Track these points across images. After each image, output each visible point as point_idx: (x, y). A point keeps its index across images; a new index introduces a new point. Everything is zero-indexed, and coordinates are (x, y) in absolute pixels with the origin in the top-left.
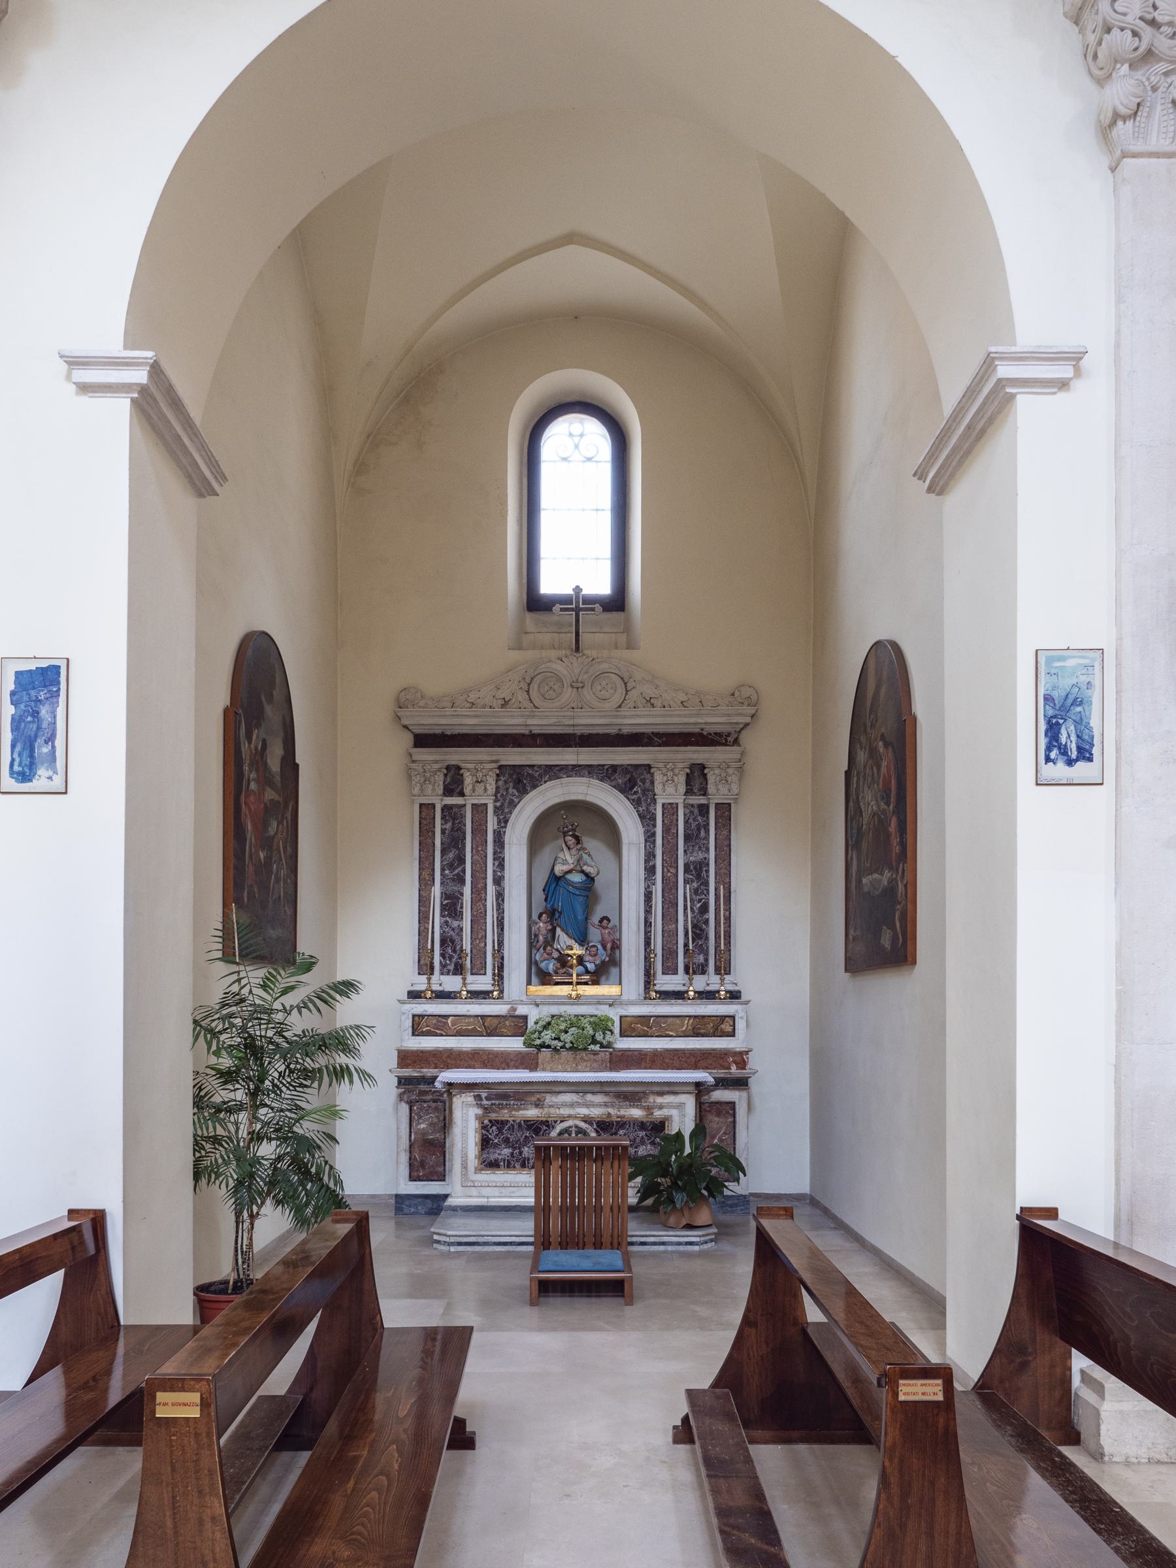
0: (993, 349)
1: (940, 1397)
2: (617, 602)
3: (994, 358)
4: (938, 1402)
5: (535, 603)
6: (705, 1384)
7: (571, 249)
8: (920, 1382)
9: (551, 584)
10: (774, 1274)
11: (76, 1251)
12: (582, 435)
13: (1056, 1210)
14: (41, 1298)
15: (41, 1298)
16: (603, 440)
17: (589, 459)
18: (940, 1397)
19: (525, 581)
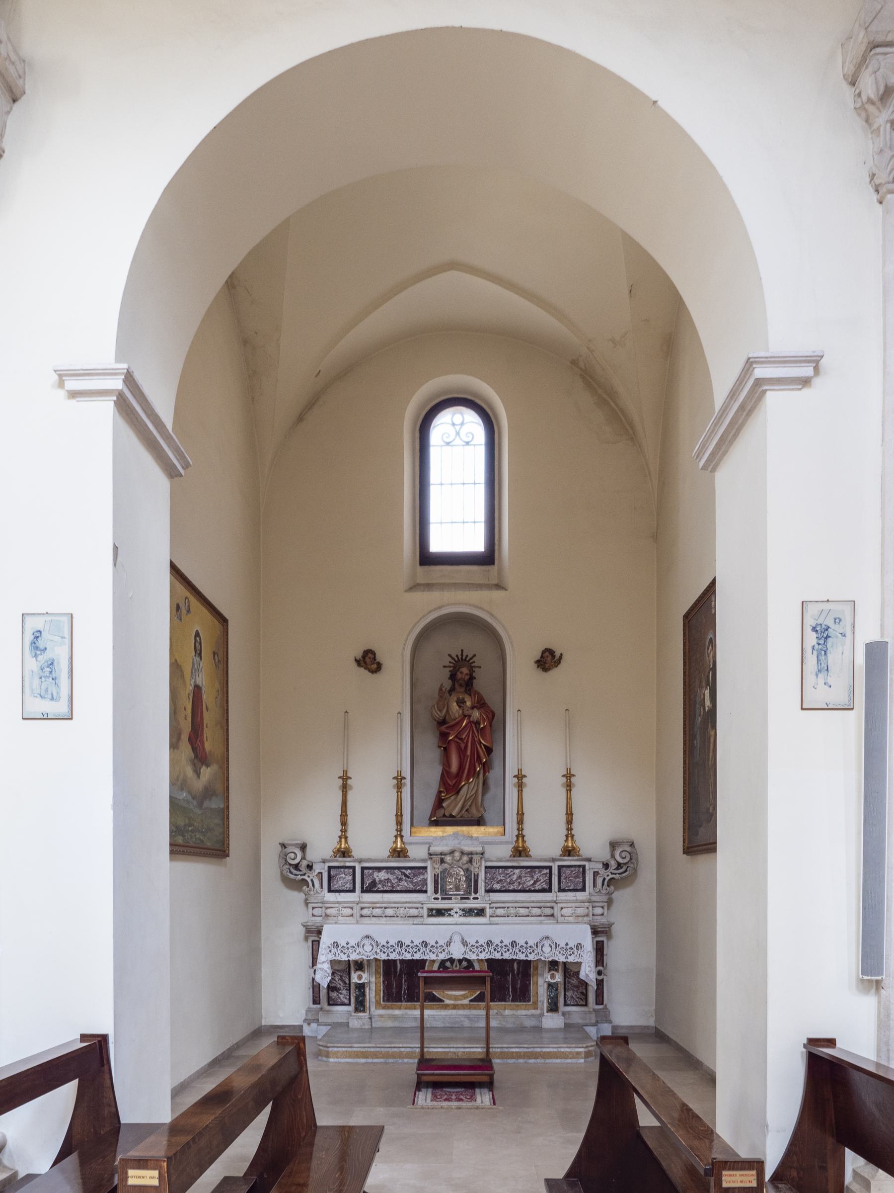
0: (750, 356)
1: (754, 1184)
2: (487, 558)
3: (752, 363)
4: (752, 1188)
5: (427, 559)
6: (560, 1173)
7: (454, 273)
8: (738, 1173)
9: (437, 544)
10: (613, 1088)
11: (87, 1065)
12: (462, 424)
13: (834, 1040)
14: (63, 1098)
15: (63, 1098)
16: (478, 426)
17: (467, 443)
18: (754, 1184)
19: (418, 541)
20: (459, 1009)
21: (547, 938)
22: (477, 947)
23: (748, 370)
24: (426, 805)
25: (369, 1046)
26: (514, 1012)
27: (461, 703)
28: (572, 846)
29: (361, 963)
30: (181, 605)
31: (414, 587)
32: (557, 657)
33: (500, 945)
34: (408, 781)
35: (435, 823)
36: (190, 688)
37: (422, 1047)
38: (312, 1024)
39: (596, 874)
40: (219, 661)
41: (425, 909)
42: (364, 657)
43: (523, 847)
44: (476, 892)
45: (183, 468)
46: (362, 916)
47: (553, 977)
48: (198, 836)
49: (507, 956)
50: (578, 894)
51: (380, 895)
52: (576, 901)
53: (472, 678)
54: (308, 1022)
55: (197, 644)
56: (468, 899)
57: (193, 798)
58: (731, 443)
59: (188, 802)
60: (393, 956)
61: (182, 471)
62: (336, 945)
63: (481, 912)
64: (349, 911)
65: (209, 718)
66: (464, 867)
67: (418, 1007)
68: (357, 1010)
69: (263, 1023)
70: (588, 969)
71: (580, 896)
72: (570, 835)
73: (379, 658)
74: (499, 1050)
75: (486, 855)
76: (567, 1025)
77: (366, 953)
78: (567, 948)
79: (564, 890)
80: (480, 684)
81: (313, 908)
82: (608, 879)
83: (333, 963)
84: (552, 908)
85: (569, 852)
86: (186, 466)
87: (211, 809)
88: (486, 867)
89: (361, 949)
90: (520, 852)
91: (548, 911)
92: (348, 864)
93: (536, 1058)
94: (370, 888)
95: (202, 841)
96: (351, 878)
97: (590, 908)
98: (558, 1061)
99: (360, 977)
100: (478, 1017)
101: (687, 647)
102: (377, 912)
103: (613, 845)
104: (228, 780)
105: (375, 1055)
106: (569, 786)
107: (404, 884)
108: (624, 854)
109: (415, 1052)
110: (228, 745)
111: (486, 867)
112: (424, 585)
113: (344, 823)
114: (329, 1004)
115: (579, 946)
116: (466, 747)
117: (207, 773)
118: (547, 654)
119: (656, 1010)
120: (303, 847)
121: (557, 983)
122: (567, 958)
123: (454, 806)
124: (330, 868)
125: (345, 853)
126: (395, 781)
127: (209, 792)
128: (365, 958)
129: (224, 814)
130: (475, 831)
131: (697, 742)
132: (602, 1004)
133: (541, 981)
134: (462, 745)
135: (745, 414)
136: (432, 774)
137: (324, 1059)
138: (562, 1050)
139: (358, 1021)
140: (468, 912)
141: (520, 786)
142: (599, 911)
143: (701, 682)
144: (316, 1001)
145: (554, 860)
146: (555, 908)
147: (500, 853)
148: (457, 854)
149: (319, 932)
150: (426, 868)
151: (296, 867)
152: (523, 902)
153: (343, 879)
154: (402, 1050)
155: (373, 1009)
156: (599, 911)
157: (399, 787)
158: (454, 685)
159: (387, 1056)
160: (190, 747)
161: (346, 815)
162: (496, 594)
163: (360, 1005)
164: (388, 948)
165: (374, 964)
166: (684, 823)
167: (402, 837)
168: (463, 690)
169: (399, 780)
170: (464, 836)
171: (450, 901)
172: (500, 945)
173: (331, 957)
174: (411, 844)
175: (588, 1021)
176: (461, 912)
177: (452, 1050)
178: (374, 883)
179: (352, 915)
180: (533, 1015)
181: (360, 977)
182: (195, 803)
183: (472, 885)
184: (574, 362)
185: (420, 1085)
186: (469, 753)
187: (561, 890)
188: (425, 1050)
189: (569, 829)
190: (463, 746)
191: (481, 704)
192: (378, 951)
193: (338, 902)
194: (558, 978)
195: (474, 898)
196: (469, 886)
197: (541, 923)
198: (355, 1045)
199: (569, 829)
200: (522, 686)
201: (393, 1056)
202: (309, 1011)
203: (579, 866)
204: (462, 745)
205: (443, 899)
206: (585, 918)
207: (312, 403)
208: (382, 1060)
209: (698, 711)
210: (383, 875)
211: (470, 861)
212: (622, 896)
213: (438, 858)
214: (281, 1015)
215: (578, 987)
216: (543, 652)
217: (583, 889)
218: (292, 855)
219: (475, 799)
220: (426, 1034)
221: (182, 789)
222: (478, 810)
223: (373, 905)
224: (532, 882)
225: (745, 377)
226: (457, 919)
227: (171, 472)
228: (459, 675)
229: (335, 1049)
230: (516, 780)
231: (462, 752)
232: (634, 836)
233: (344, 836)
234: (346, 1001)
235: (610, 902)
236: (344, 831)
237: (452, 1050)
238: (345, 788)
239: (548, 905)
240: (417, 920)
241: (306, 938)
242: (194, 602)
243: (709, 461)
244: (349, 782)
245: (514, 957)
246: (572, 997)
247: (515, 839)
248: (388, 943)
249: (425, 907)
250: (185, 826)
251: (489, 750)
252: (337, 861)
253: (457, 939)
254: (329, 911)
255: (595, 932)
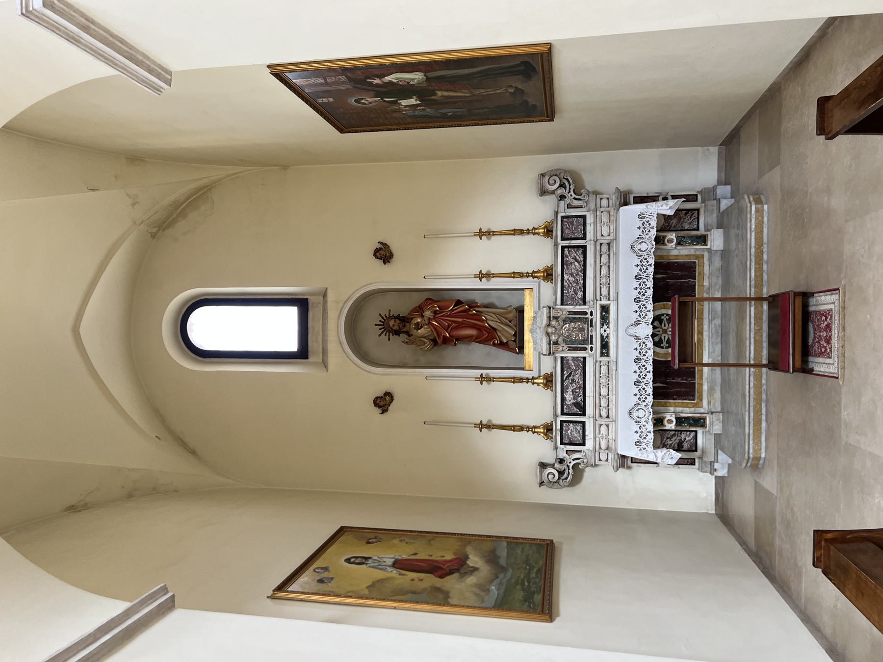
2: (302, 304)
5: (302, 353)
9: (292, 346)
20: (702, 329)
21: (632, 247)
22: (641, 311)
23: (37, 17)
24: (505, 357)
25: (748, 418)
26: (706, 277)
27: (418, 327)
28: (544, 228)
29: (655, 420)
30: (318, 578)
31: (325, 364)
32: (381, 246)
33: (639, 290)
34: (484, 372)
35: (521, 348)
36: (394, 573)
37: (750, 366)
38: (715, 467)
39: (569, 206)
40: (376, 538)
41: (601, 359)
42: (379, 407)
43: (543, 272)
44: (586, 313)
45: (165, 594)
46: (608, 417)
47: (671, 241)
48: (534, 575)
49: (650, 284)
50: (588, 222)
51: (587, 399)
52: (595, 223)
53: (398, 317)
54: (713, 471)
55: (357, 561)
56: (592, 320)
57: (497, 577)
58: (131, 47)
59: (501, 583)
60: (650, 390)
61: (169, 595)
62: (638, 443)
63: (605, 309)
64: (603, 428)
65: (424, 554)
66: (562, 324)
67: (700, 368)
68: (703, 425)
69: (713, 512)
70: (665, 207)
71: (590, 220)
72: (533, 231)
73: (380, 394)
74: (753, 289)
75: (551, 305)
76: (719, 226)
77: (646, 415)
78: (643, 228)
79: (585, 234)
80: (404, 312)
81: (600, 460)
82: (574, 195)
83: (656, 447)
84: (601, 244)
85: (549, 232)
86: (165, 590)
87: (507, 557)
88: (562, 304)
89: (643, 420)
90: (548, 274)
91: (605, 248)
92: (559, 427)
93: (762, 252)
94: (581, 409)
95: (539, 571)
96: (571, 425)
97: (602, 209)
98: (765, 230)
99: (670, 421)
100: (712, 311)
101: (367, 128)
102: (604, 402)
103: (543, 192)
104: (481, 536)
105: (758, 412)
106: (490, 234)
107: (578, 377)
108: (552, 182)
109: (755, 372)
110: (449, 534)
111: (562, 304)
112: (323, 356)
113: (521, 428)
114: (696, 450)
115: (641, 216)
116: (455, 322)
117: (474, 560)
118: (378, 254)
119: (702, 146)
120: (543, 466)
121: (677, 237)
122: (653, 228)
123: (507, 333)
124: (562, 443)
125: (548, 429)
126: (484, 383)
127: (492, 559)
128: (651, 416)
129: (513, 542)
130: (528, 315)
131: (449, 111)
132: (696, 195)
133: (675, 252)
134: (454, 326)
135: (93, 27)
136: (479, 352)
137: (761, 462)
138: (753, 227)
139: (715, 425)
140: (605, 320)
141: (489, 276)
142: (604, 202)
143: (395, 111)
144: (693, 463)
145: (556, 244)
146: (602, 241)
147: (548, 292)
148: (550, 330)
149: (623, 457)
150: (562, 358)
151: (561, 473)
152: (595, 271)
153: (573, 432)
154: (752, 384)
155: (702, 410)
156: (604, 202)
157: (489, 379)
158: (404, 332)
159: (758, 400)
160: (448, 577)
161: (514, 426)
162: (330, 297)
163: (699, 422)
164: (641, 395)
165: (656, 408)
166: (524, 122)
167: (533, 378)
168: (407, 325)
169: (482, 379)
170: (533, 324)
171: (594, 337)
172: (639, 290)
173: (650, 448)
174: (540, 371)
175: (715, 208)
176: (605, 327)
177: (752, 336)
178: (576, 404)
179: (607, 426)
180: (710, 259)
181: (670, 421)
182: (501, 576)
183: (580, 317)
184: (153, 236)
185: (805, 369)
186: (460, 320)
187: (584, 237)
188: (752, 362)
189: (528, 232)
190: (454, 325)
191: (420, 310)
192: (644, 404)
193: (595, 438)
194: (672, 236)
195: (591, 315)
196: (580, 320)
197: (616, 254)
198: (747, 431)
199: (528, 232)
200: (405, 276)
201: (758, 394)
202: (701, 469)
203: (562, 221)
204: (454, 326)
205: (591, 343)
206: (612, 213)
207: (182, 443)
208: (763, 405)
209: (421, 113)
210: (569, 397)
211: (556, 318)
212: (590, 182)
213: (553, 347)
214: (705, 495)
215: (680, 219)
216: (377, 257)
217: (584, 217)
218: (551, 476)
219: (500, 314)
220: (731, 361)
221: (489, 590)
222: (510, 312)
223: (597, 406)
224: (576, 263)
225: (48, 22)
226: (611, 331)
227: (169, 606)
228: (396, 328)
229: (751, 451)
230: (484, 279)
231: (460, 326)
232: (535, 175)
233: (532, 429)
234: (693, 434)
235: (596, 193)
236: (528, 429)
237: (752, 336)
238: (490, 426)
239: (598, 248)
240: (613, 367)
241: (629, 468)
242: (318, 563)
243: (158, 76)
244: (484, 422)
245: (652, 277)
246: (690, 223)
247: (536, 279)
248: (636, 395)
249: (599, 359)
250: (523, 590)
251: (459, 303)
252: (556, 436)
253: (632, 330)
254: (603, 446)
255: (626, 203)
